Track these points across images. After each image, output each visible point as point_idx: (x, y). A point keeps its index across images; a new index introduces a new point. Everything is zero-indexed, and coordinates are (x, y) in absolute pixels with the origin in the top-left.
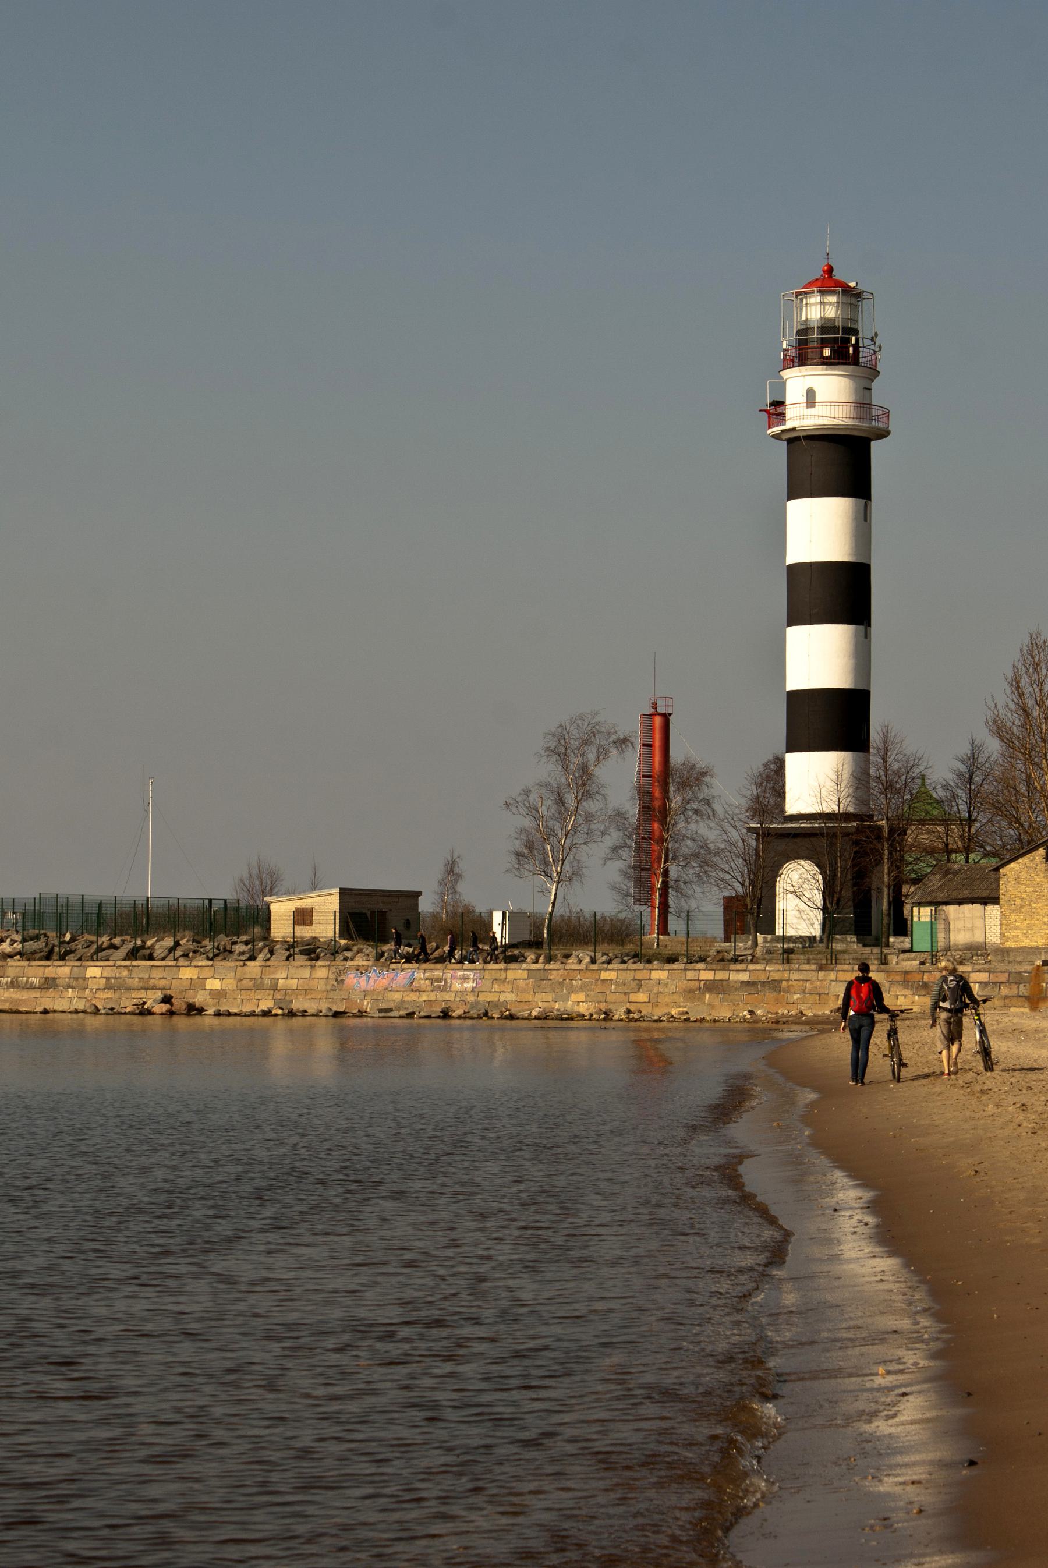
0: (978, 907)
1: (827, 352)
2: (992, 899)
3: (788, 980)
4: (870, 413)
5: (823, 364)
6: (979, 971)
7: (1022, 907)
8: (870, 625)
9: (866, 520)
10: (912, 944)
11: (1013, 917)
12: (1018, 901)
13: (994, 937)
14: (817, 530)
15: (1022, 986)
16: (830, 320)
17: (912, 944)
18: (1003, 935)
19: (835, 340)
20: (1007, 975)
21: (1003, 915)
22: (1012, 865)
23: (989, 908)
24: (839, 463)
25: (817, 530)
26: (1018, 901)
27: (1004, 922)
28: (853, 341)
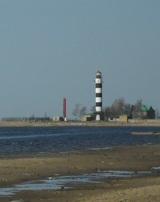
2: (119, 118)
14: (98, 91)
24: (100, 86)
25: (98, 91)
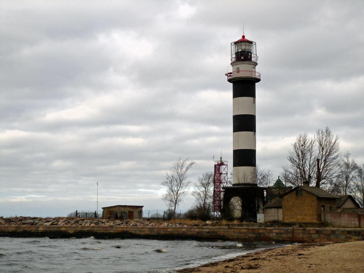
0: (276, 209)
1: (242, 58)
3: (220, 232)
4: (255, 74)
5: (241, 61)
6: (276, 229)
7: (289, 209)
8: (255, 131)
9: (254, 103)
10: (175, 209)
11: (287, 212)
12: (288, 207)
13: (281, 218)
15: (288, 234)
16: (243, 49)
17: (175, 209)
18: (283, 218)
19: (245, 54)
20: (284, 230)
21: (283, 212)
22: (286, 196)
23: (279, 209)
26: (288, 207)
27: (284, 214)
28: (250, 54)
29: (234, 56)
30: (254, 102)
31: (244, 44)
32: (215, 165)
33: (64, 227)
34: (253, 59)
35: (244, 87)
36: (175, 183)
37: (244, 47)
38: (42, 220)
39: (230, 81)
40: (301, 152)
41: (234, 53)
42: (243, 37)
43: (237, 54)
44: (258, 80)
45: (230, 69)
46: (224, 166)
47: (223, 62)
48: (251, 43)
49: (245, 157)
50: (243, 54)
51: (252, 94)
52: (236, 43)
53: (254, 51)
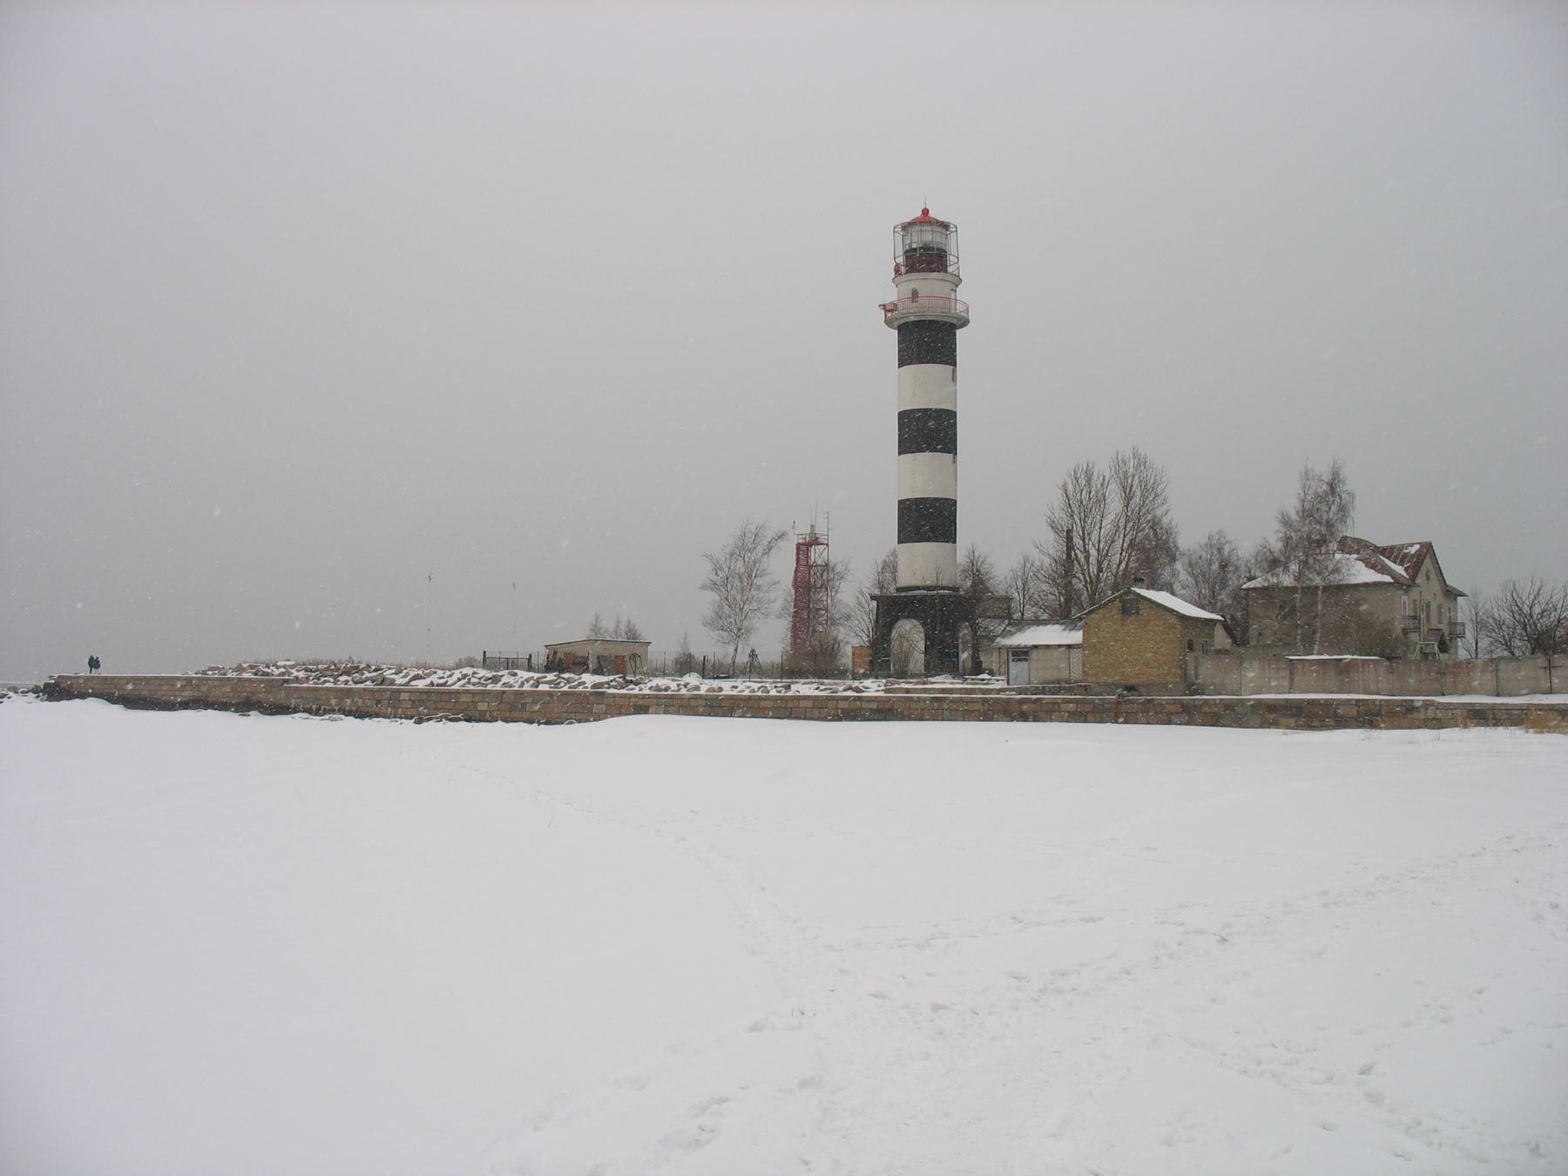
8: (954, 364)
29: (901, 260)
30: (955, 461)
31: (928, 228)
32: (799, 545)
33: (468, 692)
34: (950, 269)
35: (928, 340)
36: (737, 582)
37: (928, 236)
38: (749, 577)
39: (889, 323)
40: (1081, 502)
41: (900, 252)
42: (925, 212)
43: (910, 254)
44: (965, 323)
45: (892, 295)
46: (821, 547)
47: (878, 281)
48: (945, 226)
49: (928, 519)
50: (926, 256)
51: (949, 358)
52: (906, 227)
53: (952, 250)
